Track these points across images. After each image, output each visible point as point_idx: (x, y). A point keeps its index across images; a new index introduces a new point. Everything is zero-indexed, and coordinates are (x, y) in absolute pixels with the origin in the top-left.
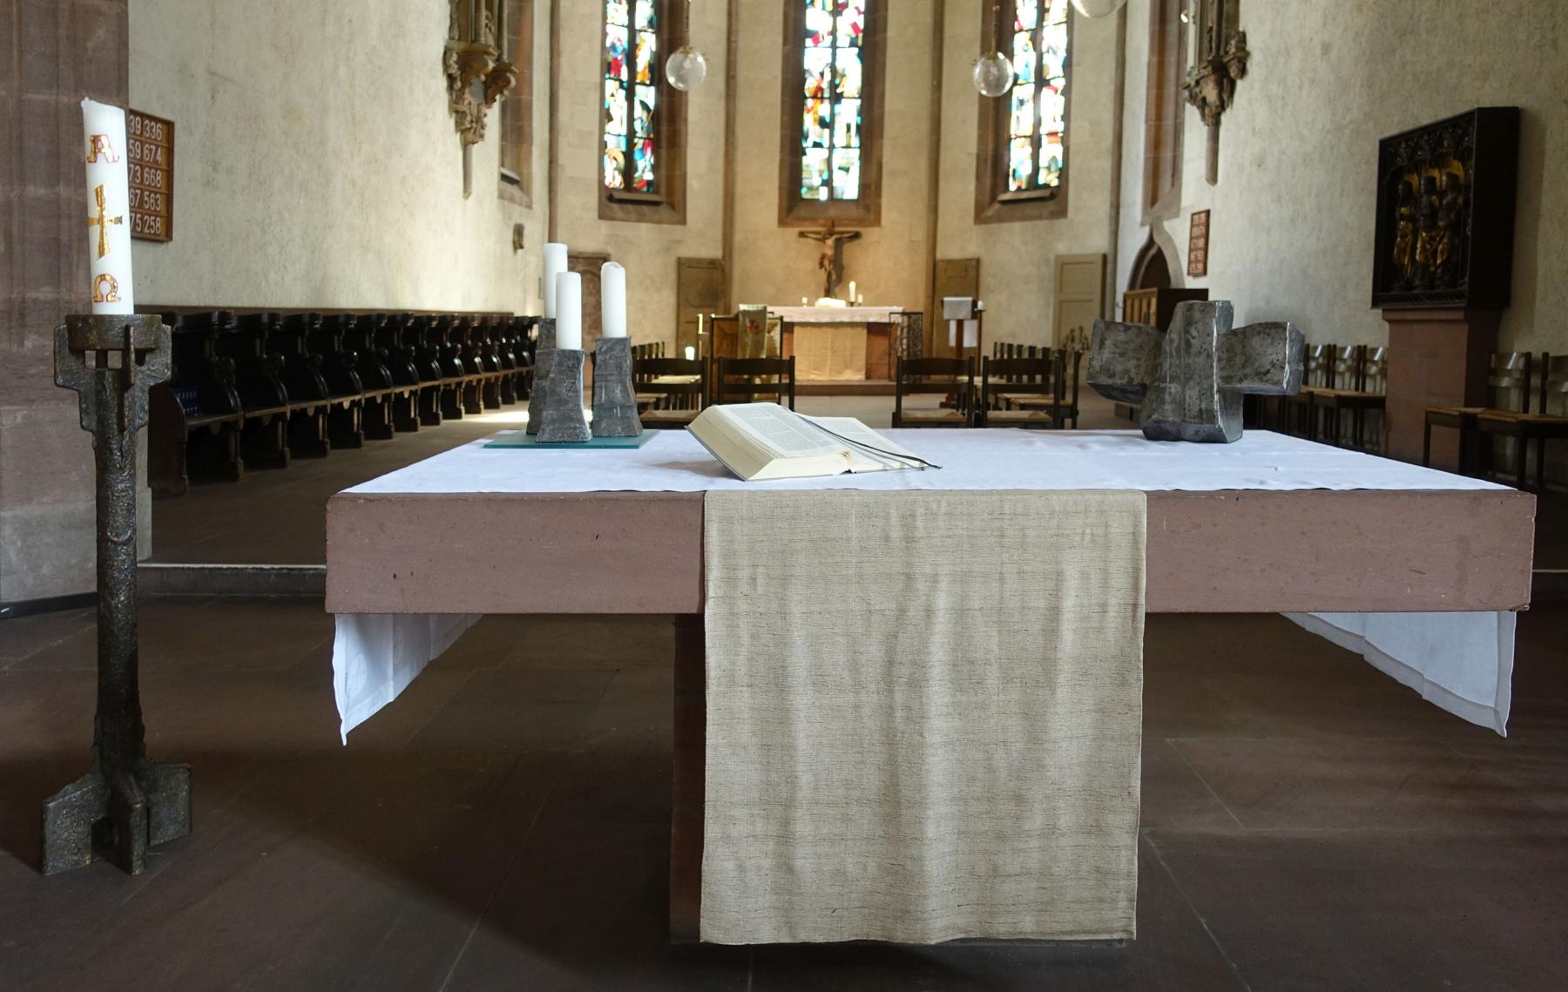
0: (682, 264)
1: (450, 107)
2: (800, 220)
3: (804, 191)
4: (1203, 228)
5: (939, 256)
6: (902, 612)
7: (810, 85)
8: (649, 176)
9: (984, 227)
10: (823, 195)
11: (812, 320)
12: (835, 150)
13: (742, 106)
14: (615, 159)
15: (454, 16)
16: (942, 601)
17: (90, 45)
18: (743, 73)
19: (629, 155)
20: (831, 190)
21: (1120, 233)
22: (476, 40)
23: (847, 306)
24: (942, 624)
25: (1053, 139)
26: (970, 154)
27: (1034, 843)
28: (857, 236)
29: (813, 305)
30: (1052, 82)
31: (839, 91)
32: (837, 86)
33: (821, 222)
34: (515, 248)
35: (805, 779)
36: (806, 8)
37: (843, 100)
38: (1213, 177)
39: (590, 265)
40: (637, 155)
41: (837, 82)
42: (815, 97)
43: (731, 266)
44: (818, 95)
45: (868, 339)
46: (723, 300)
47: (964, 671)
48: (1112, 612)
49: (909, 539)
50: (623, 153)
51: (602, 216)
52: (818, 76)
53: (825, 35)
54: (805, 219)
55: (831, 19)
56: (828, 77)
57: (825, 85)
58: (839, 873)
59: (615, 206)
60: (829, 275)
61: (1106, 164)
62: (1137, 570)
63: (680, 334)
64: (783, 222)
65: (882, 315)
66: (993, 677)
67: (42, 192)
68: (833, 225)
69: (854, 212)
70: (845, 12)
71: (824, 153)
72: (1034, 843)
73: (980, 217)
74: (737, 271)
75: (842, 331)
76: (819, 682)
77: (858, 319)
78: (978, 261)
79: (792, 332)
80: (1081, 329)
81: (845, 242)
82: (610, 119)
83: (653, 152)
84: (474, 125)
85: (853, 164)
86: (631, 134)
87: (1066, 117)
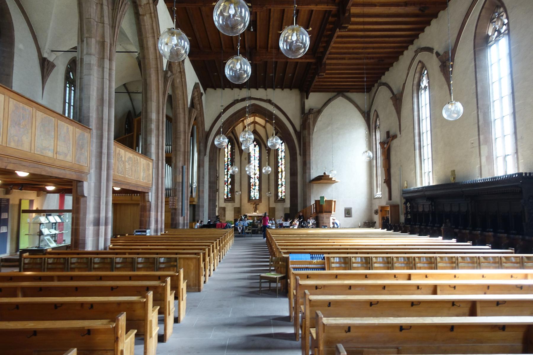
0: (235, 208)
7: (252, 184)
8: (230, 197)
10: (254, 198)
18: (242, 183)
19: (227, 194)
28: (258, 204)
44: (253, 185)
55: (114, 290)
56: (254, 183)
57: (254, 184)
69: (258, 201)
73: (275, 202)
86: (228, 192)
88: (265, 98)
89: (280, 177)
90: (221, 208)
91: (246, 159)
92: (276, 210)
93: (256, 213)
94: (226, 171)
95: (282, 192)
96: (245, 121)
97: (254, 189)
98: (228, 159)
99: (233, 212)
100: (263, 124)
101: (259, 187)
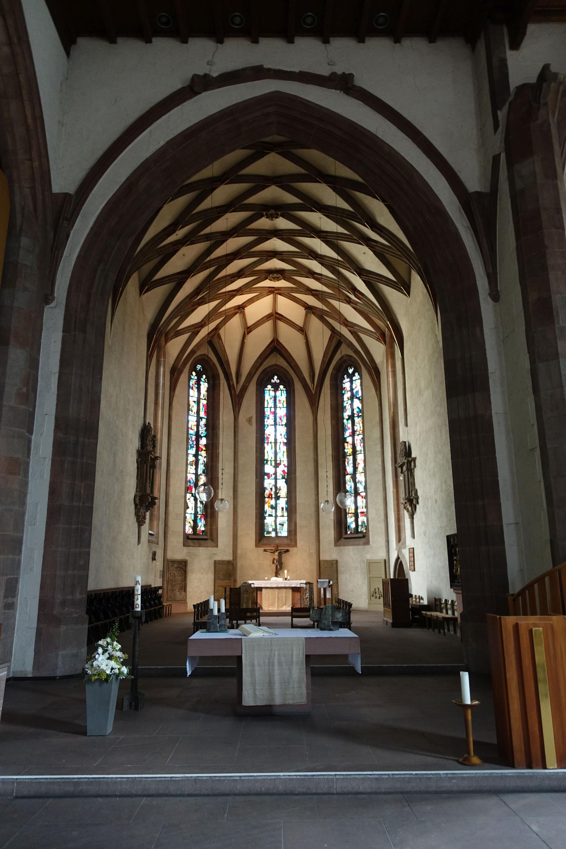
0: (217, 564)
1: (135, 514)
2: (264, 545)
3: (265, 533)
4: (412, 554)
5: (321, 558)
6: (270, 655)
7: (267, 492)
8: (203, 529)
9: (338, 548)
11: (269, 586)
12: (278, 517)
13: (240, 501)
14: (190, 523)
15: (138, 484)
16: (276, 653)
17: (84, 537)
19: (195, 521)
20: (277, 533)
21: (390, 551)
22: (145, 491)
23: (283, 580)
24: (276, 657)
25: (363, 514)
26: (331, 520)
27: (291, 689)
28: (287, 551)
29: (270, 580)
30: (361, 494)
31: (278, 495)
32: (278, 493)
33: (273, 545)
34: (153, 560)
35: (257, 680)
36: (264, 465)
37: (280, 499)
38: (413, 537)
39: (179, 564)
40: (198, 521)
41: (277, 492)
42: (269, 497)
43: (236, 563)
44: (270, 496)
45: (292, 593)
46: (233, 577)
47: (280, 664)
48: (301, 655)
49: (271, 644)
50: (192, 520)
51: (184, 545)
52: (270, 490)
53: (272, 475)
54: (266, 544)
56: (274, 490)
57: (273, 493)
58: (263, 694)
59: (189, 541)
60: (277, 566)
61: (383, 525)
62: (304, 648)
63: (216, 591)
64: (257, 546)
65: (297, 584)
66: (284, 664)
67: (71, 572)
68: (278, 547)
69: (286, 541)
70: (280, 466)
71: (273, 518)
72: (291, 689)
74: (239, 564)
75: (282, 590)
76: (259, 665)
77: (287, 586)
78: (337, 561)
79: (262, 591)
80: (379, 589)
81: (283, 553)
82: (188, 508)
83: (204, 520)
84: (143, 519)
85: (285, 522)
87: (366, 507)
88: (325, 71)
89: (350, 469)
90: (173, 562)
91: (249, 421)
92: (340, 568)
93: (280, 580)
94: (192, 451)
95: (356, 515)
96: (248, 310)
97: (274, 508)
98: (199, 419)
99: (211, 576)
100: (299, 322)
101: (287, 503)
